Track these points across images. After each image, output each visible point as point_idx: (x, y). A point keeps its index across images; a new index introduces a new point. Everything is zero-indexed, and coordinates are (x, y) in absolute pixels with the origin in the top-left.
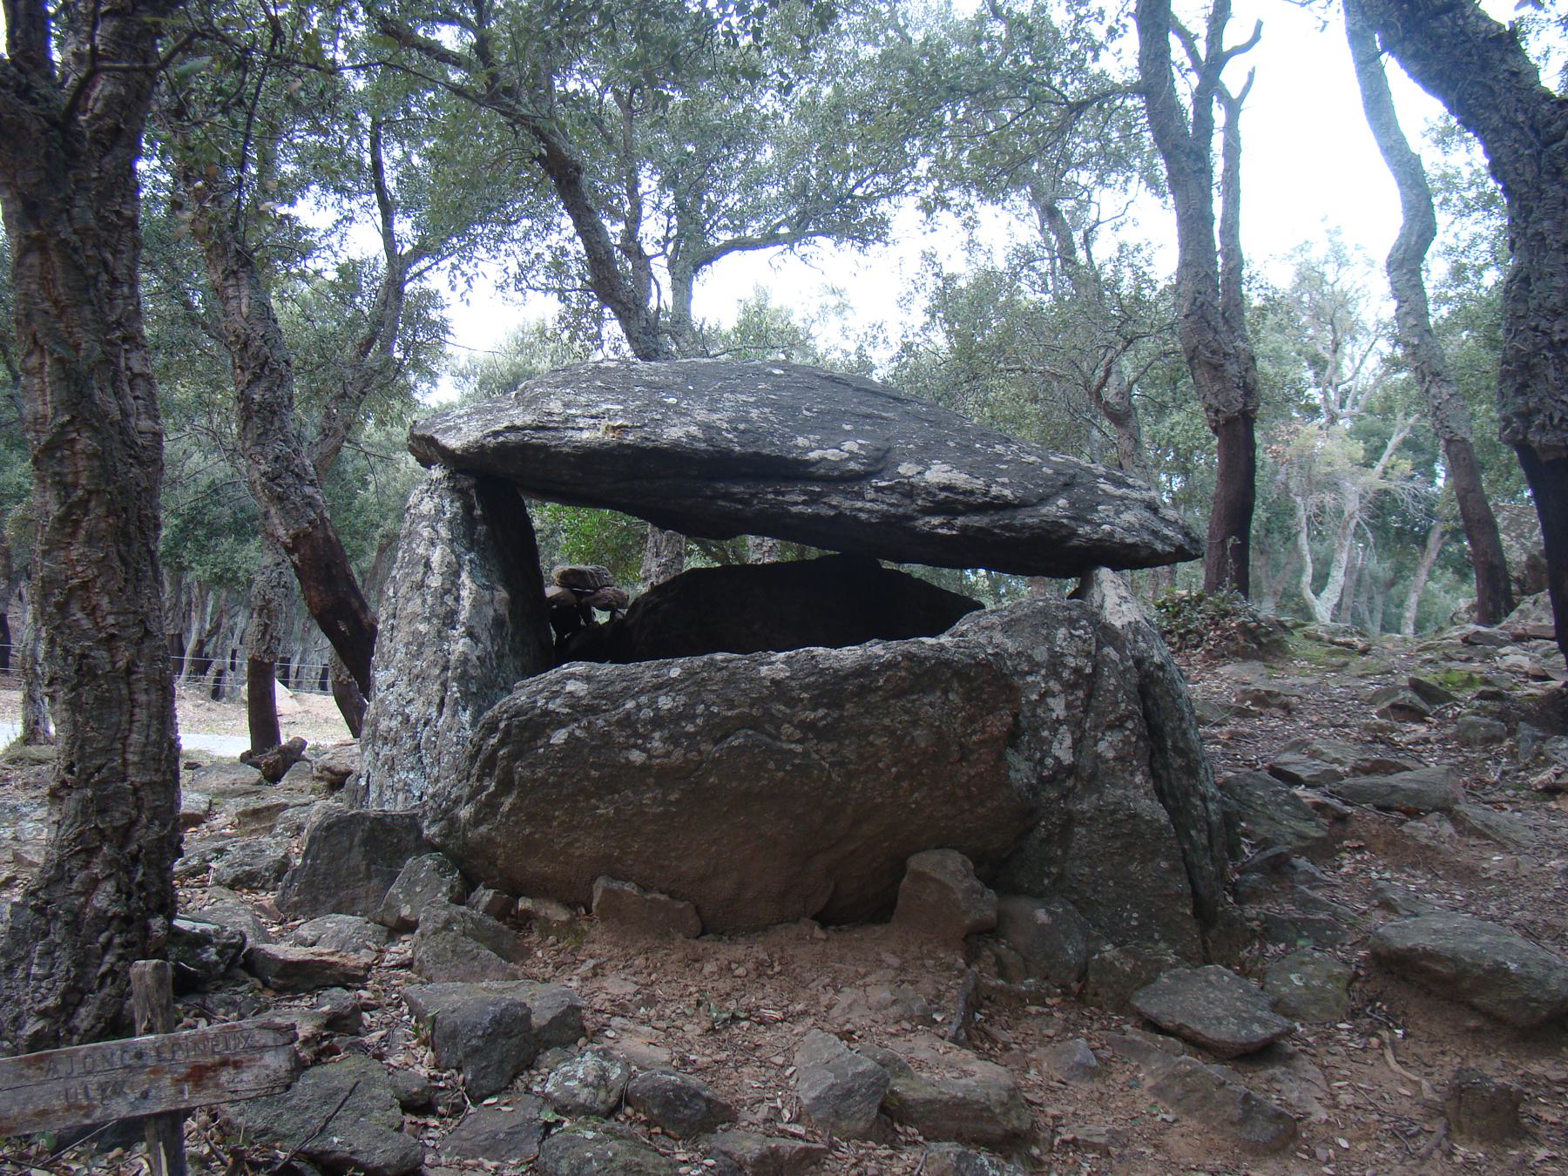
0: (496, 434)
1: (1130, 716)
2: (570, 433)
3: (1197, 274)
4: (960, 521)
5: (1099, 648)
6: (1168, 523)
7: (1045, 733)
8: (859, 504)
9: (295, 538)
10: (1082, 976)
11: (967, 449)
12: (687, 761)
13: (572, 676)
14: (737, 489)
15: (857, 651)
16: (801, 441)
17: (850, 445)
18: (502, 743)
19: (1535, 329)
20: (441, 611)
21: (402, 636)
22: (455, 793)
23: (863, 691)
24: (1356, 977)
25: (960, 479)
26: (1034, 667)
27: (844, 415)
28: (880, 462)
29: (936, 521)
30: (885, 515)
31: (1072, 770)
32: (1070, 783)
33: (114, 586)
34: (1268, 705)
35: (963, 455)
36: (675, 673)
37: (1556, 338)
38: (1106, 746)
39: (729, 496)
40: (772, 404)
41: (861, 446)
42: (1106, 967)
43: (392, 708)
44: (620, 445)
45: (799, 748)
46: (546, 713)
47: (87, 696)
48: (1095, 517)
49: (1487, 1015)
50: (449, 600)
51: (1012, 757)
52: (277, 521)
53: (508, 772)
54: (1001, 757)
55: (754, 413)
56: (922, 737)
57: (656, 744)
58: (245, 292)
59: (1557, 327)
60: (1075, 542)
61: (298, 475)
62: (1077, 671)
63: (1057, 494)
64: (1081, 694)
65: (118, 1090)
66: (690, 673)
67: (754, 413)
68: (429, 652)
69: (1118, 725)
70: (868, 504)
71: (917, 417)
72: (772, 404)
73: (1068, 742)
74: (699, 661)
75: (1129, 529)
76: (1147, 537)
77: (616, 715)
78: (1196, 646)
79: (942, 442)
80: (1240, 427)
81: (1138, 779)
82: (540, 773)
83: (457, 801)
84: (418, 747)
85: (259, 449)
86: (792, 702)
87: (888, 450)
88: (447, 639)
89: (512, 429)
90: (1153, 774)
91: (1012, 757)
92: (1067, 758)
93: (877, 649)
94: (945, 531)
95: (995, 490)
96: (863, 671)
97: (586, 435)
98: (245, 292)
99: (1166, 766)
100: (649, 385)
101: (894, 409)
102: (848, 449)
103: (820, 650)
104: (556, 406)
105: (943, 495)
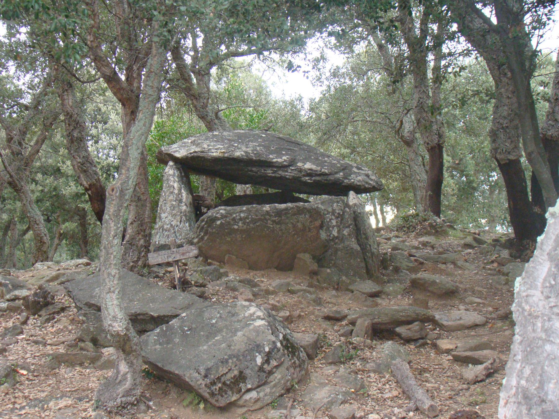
0: (191, 153)
1: (351, 224)
2: (210, 153)
3: (420, 91)
4: (313, 178)
5: (344, 208)
6: (372, 180)
7: (331, 229)
8: (287, 174)
9: (90, 185)
10: (338, 284)
11: (317, 159)
12: (247, 228)
13: (221, 209)
14: (254, 169)
15: (285, 205)
16: (271, 156)
17: (285, 158)
18: (205, 224)
19: (499, 122)
20: (178, 199)
21: (168, 205)
22: (193, 236)
23: (286, 214)
24: (406, 288)
25: (314, 167)
26: (328, 213)
27: (282, 149)
28: (292, 163)
29: (307, 178)
30: (293, 176)
31: (337, 238)
32: (337, 241)
33: (144, 183)
34: (426, 246)
35: (316, 161)
36: (244, 209)
37: (504, 126)
38: (346, 232)
39: (251, 171)
40: (263, 146)
41: (287, 158)
42: (343, 282)
43: (167, 223)
44: (224, 157)
45: (272, 226)
46: (216, 217)
47: (139, 204)
48: (350, 178)
49: (432, 292)
50: (180, 196)
51: (321, 232)
52: (83, 179)
53: (207, 230)
54: (318, 232)
55: (258, 148)
56: (300, 225)
57: (240, 224)
58: (70, 97)
59: (505, 122)
60: (344, 184)
61: (90, 163)
62: (339, 214)
63: (340, 172)
64: (339, 219)
65: (170, 256)
66: (248, 209)
67: (258, 148)
68: (177, 209)
69: (349, 227)
70: (289, 174)
71: (304, 149)
72: (263, 146)
73: (336, 231)
74: (250, 206)
75: (359, 181)
76: (363, 183)
77: (231, 218)
78: (413, 232)
79: (310, 157)
80: (437, 150)
81: (353, 240)
82: (214, 230)
83: (193, 238)
84: (175, 232)
85: (77, 154)
86: (271, 216)
87: (295, 159)
88: (180, 206)
89: (195, 152)
90: (358, 240)
91: (321, 232)
92: (336, 234)
93: (289, 205)
94: (309, 181)
95: (323, 170)
96: (286, 209)
97: (214, 154)
98: (70, 97)
99: (361, 238)
100: (229, 140)
101: (297, 147)
102: (284, 159)
103: (276, 205)
104: (205, 146)
105: (309, 171)
